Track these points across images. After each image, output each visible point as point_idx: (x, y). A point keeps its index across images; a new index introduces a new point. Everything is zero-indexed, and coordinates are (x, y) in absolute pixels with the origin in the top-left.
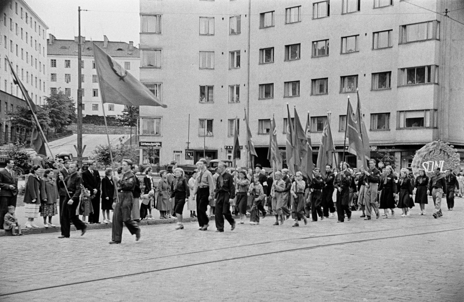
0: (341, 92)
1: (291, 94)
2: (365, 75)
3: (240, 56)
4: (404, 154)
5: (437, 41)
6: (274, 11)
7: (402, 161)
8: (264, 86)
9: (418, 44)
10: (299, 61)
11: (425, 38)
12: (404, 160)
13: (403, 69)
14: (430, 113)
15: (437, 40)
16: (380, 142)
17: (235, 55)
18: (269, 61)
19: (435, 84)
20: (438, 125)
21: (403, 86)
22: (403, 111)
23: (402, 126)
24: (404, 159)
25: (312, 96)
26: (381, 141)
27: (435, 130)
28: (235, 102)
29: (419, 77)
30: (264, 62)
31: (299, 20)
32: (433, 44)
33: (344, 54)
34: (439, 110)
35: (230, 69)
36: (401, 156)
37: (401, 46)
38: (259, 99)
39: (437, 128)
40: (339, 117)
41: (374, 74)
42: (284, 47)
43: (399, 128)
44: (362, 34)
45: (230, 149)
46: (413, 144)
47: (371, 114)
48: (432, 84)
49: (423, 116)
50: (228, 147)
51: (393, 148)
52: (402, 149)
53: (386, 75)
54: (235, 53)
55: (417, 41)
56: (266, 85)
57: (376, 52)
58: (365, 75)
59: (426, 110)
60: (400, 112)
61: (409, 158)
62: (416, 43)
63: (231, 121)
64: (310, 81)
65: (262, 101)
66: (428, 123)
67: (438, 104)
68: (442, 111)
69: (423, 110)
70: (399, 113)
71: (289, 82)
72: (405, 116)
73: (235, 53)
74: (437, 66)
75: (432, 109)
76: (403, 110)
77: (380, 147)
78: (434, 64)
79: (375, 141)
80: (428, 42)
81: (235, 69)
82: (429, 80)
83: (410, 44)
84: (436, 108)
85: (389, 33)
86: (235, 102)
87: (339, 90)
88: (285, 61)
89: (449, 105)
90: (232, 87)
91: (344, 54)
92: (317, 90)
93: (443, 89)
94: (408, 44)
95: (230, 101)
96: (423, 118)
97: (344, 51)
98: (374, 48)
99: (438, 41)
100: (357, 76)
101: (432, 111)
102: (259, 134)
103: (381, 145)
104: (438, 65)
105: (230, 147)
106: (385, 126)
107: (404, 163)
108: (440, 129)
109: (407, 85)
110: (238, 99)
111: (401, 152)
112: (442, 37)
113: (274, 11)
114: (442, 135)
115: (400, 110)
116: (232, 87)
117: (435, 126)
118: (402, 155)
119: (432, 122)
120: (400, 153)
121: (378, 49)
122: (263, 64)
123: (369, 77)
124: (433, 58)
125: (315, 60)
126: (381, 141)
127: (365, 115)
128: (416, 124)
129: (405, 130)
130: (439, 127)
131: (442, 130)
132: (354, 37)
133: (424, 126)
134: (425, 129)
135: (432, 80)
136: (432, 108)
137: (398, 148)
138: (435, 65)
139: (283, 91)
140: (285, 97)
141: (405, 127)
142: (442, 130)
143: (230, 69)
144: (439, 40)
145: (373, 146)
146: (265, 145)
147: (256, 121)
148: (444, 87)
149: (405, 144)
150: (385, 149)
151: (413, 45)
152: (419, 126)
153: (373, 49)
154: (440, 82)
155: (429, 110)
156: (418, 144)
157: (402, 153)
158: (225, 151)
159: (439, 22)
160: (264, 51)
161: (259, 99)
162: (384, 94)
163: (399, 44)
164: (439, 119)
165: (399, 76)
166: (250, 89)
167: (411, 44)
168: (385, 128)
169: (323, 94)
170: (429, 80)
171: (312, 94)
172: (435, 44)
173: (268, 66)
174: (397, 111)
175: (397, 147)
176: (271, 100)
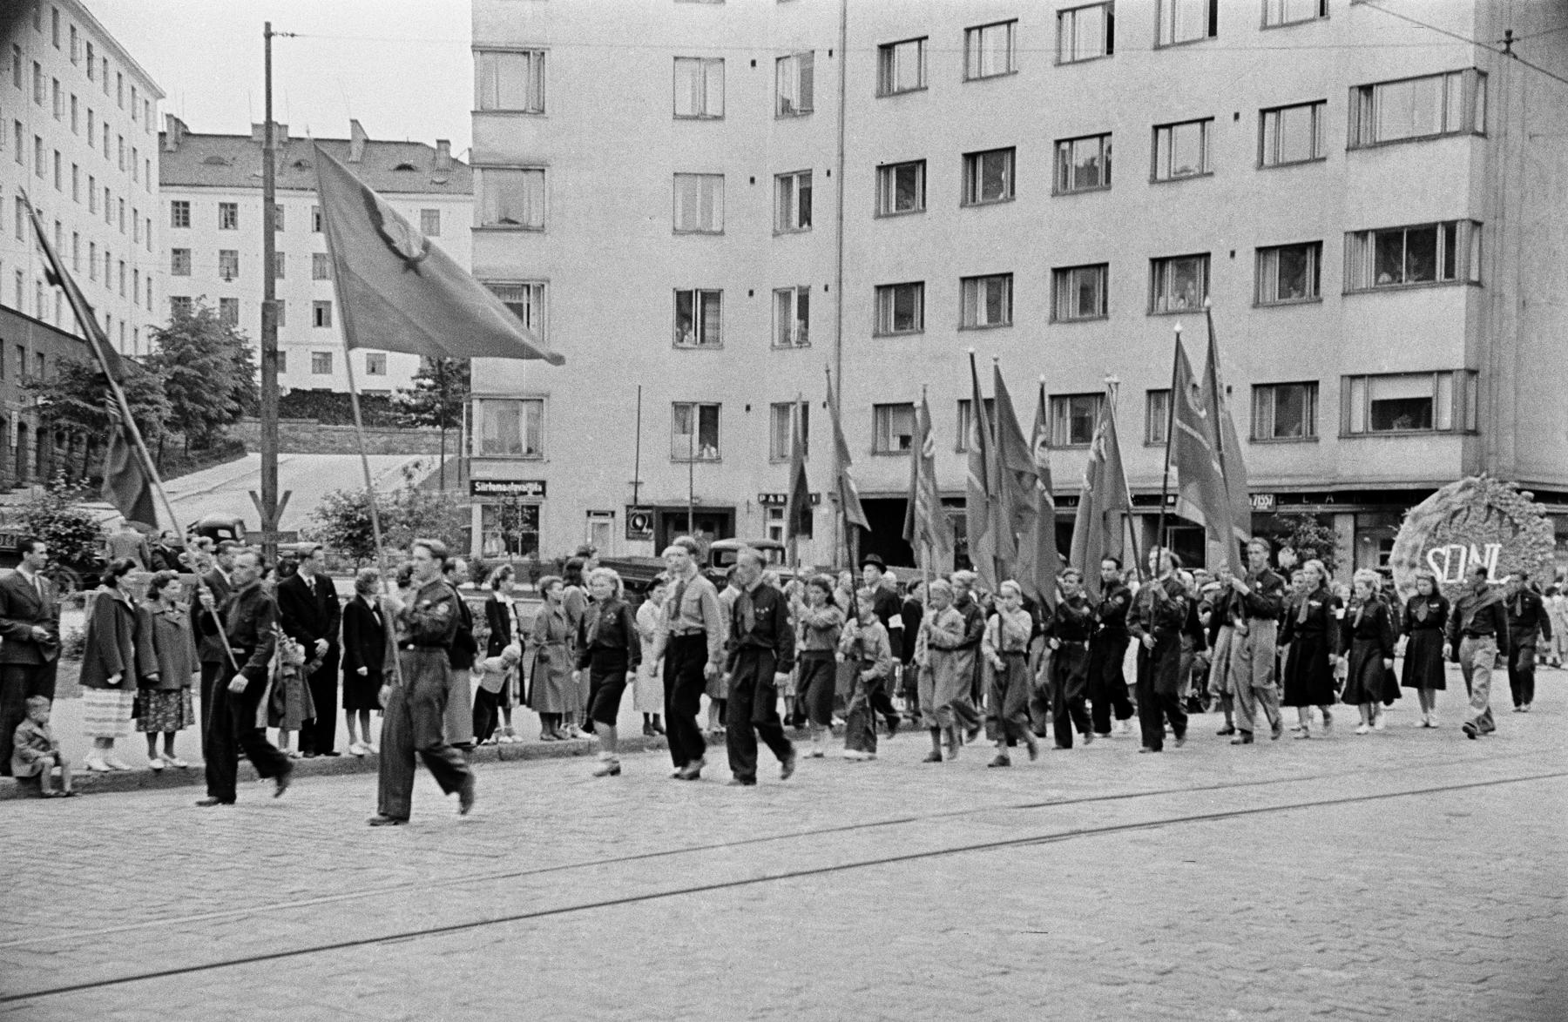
0: (1151, 312)
1: (983, 319)
2: (1233, 254)
3: (809, 190)
4: (1364, 521)
5: (1475, 138)
6: (926, 38)
7: (1360, 546)
8: (893, 291)
9: (1411, 149)
10: (1010, 205)
11: (1438, 130)
12: (1365, 543)
13: (1362, 235)
14: (1454, 383)
15: (1476, 134)
16: (1286, 481)
17: (796, 186)
18: (908, 207)
19: (1471, 283)
20: (1481, 423)
21: (1363, 292)
22: (1361, 377)
23: (1358, 426)
24: (1367, 539)
25: (1056, 326)
26: (1289, 476)
27: (1472, 439)
28: (794, 344)
29: (1414, 262)
30: (893, 209)
31: (1012, 69)
32: (1462, 147)
33: (1163, 182)
34: (1485, 372)
35: (776, 234)
36: (1357, 529)
37: (1356, 154)
38: (876, 335)
39: (1475, 433)
40: (1144, 396)
41: (1262, 251)
42: (960, 160)
43: (1347, 435)
44: (1223, 116)
45: (776, 503)
46: (1396, 487)
47: (1255, 387)
48: (1458, 284)
49: (1429, 394)
50: (772, 499)
51: (1329, 502)
52: (1357, 503)
53: (1304, 253)
54: (796, 180)
55: (1410, 140)
56: (897, 287)
57: (1269, 176)
58: (1233, 254)
59: (1441, 373)
60: (1353, 377)
61: (1382, 533)
62: (1405, 146)
63: (782, 409)
64: (1049, 274)
65: (887, 342)
66: (1445, 416)
67: (1480, 351)
68: (1495, 374)
69: (1429, 373)
70: (1347, 381)
71: (975, 279)
72: (1367, 393)
73: (796, 180)
74: (1477, 224)
75: (1458, 370)
76: (1362, 372)
77: (1283, 498)
78: (1466, 216)
79: (1267, 476)
80: (1445, 143)
81: (795, 232)
82: (1449, 272)
83: (1385, 149)
84: (1472, 367)
85: (1314, 111)
86: (794, 344)
87: (1145, 304)
88: (962, 206)
89: (1518, 356)
90: (785, 296)
91: (1163, 182)
92: (1072, 306)
93: (1496, 300)
94: (1379, 149)
95: (777, 343)
96: (1429, 400)
97: (1162, 174)
98: (1262, 163)
99: (1481, 140)
100: (1206, 256)
101: (1460, 377)
102: (874, 453)
103: (1287, 490)
104: (1479, 219)
105: (776, 496)
106: (1300, 428)
107: (1366, 553)
108: (1488, 438)
109: (1376, 289)
110: (804, 335)
111: (1355, 514)
112: (1493, 127)
113: (926, 38)
114: (1493, 458)
115: (1352, 372)
116: (785, 296)
117: (1471, 426)
118: (1360, 524)
119: (1460, 414)
120: (1351, 519)
121: (1278, 166)
122: (888, 216)
123: (1247, 259)
124: (1463, 198)
125: (1066, 203)
126: (1289, 476)
127: (1234, 390)
128: (1406, 418)
129: (1369, 441)
130: (1484, 428)
131: (1493, 440)
132: (1198, 126)
133: (1434, 426)
134: (1436, 438)
135: (1459, 272)
136: (1460, 365)
137: (1345, 502)
138: (1469, 220)
139: (956, 308)
140: (961, 328)
141: (1370, 429)
142: (1493, 440)
143: (776, 234)
144: (1483, 135)
145: (1259, 494)
146: (895, 489)
147: (865, 410)
148: (1501, 295)
149: (1368, 487)
150: (1301, 503)
151: (1396, 153)
152: (1415, 425)
153: (1261, 165)
154: (1487, 279)
155: (1450, 372)
156: (1411, 487)
157: (1360, 516)
158: (762, 511)
159: (1483, 75)
160: (894, 173)
161: (876, 335)
162: (1298, 317)
163: (1348, 150)
164: (1484, 404)
165: (1349, 256)
166: (846, 301)
167: (1390, 148)
168: (1299, 432)
169: (1091, 319)
170: (1449, 272)
171: (1054, 319)
172: (1468, 149)
173: (905, 223)
174: (1342, 377)
175: (1342, 497)
176: (915, 340)
